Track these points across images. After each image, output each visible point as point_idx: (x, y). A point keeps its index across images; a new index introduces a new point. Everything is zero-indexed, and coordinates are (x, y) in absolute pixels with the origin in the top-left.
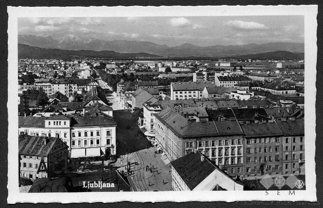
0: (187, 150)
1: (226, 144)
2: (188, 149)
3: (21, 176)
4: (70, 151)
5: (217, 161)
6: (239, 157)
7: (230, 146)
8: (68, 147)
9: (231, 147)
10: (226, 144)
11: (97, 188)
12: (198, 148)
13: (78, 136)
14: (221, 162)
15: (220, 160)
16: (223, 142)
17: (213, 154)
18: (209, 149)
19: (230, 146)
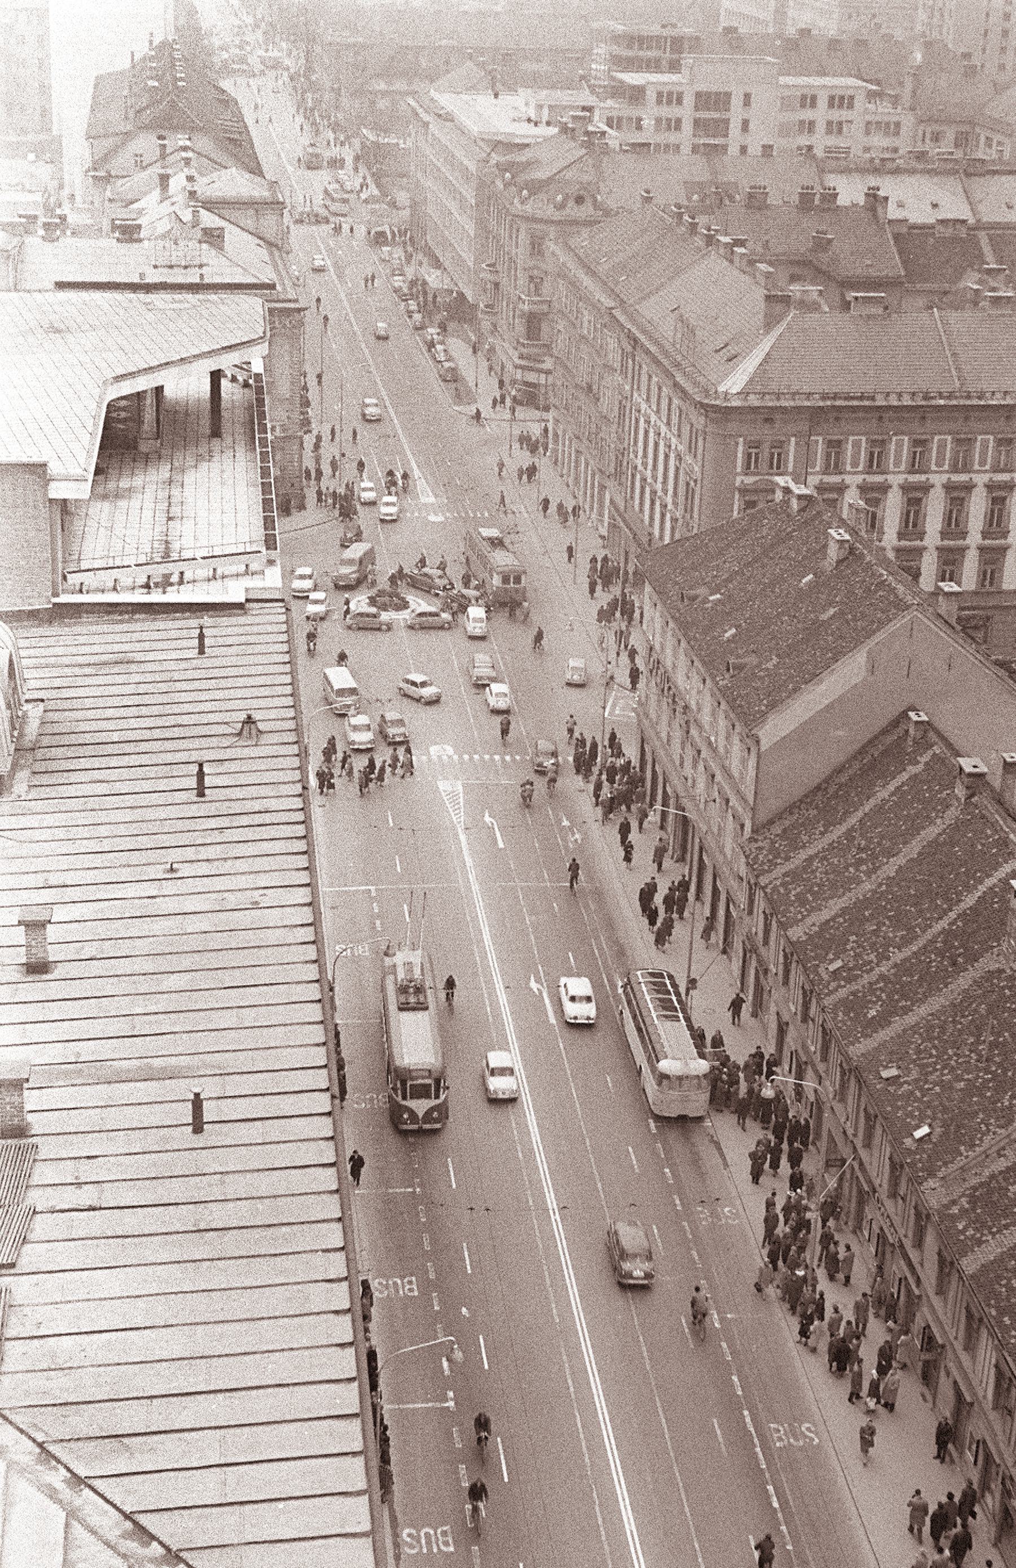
0: (744, 491)
1: (875, 462)
2: (750, 480)
3: (902, 1262)
4: (250, 223)
5: (929, 565)
6: (950, 550)
7: (895, 480)
8: (389, 83)
9: (949, 487)
10: (875, 462)
11: (423, 1526)
12: (813, 480)
13: (702, 87)
14: (952, 573)
15: (950, 562)
16: (899, 448)
17: (912, 524)
18: (969, 487)
19: (895, 480)
